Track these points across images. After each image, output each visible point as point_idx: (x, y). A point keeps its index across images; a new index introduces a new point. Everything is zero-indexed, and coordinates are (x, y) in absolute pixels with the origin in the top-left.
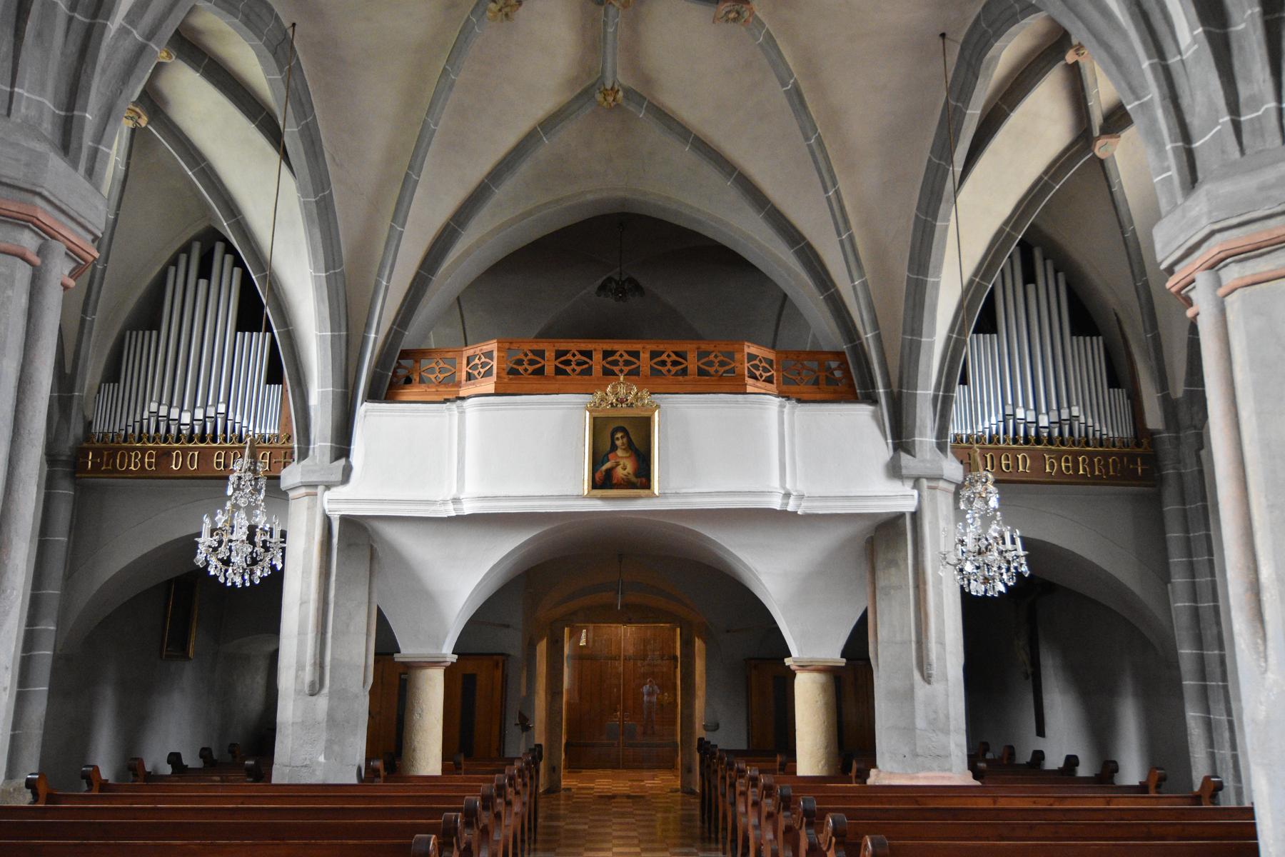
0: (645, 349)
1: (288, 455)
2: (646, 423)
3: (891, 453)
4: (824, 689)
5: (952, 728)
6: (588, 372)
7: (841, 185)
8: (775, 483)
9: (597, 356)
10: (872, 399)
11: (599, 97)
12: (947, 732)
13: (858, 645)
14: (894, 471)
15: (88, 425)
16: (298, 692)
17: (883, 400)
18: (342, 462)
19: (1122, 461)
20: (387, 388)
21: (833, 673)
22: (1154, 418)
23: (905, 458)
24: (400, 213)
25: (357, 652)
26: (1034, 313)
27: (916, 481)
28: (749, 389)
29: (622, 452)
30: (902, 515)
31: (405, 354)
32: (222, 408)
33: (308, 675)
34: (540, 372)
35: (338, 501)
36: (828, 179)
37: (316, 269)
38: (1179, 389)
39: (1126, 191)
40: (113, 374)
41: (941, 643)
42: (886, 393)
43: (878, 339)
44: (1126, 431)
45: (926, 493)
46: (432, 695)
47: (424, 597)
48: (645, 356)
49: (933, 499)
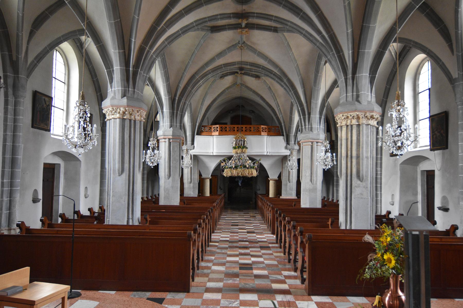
0: (244, 126)
1: (183, 144)
4: (274, 183)
6: (234, 131)
7: (278, 100)
8: (266, 150)
9: (236, 128)
10: (283, 135)
12: (292, 190)
13: (280, 177)
14: (286, 148)
16: (165, 177)
20: (199, 133)
21: (275, 180)
23: (288, 146)
24: (202, 104)
25: (196, 177)
27: (290, 150)
28: (262, 134)
31: (203, 126)
33: (189, 180)
34: (226, 131)
36: (275, 99)
41: (292, 176)
43: (285, 125)
47: (206, 168)
48: (244, 128)
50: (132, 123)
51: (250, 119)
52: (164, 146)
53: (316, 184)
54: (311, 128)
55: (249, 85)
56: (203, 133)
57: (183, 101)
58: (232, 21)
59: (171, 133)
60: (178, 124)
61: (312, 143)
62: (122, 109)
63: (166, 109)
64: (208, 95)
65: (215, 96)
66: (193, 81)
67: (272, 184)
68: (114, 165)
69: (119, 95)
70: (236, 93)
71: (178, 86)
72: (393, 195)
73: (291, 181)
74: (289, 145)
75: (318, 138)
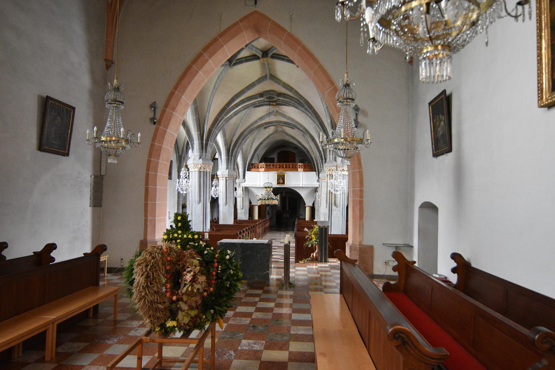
0: (284, 164)
2: (284, 176)
10: (316, 171)
13: (313, 204)
20: (249, 170)
24: (251, 147)
25: (247, 205)
29: (281, 179)
50: (205, 173)
51: (294, 154)
52: (222, 183)
55: (287, 132)
56: (253, 170)
57: (236, 149)
58: (268, 103)
59: (227, 173)
60: (232, 167)
62: (200, 166)
63: (224, 156)
64: (255, 143)
65: (261, 141)
66: (243, 136)
67: (308, 210)
68: (195, 198)
69: (197, 158)
70: (279, 137)
71: (232, 140)
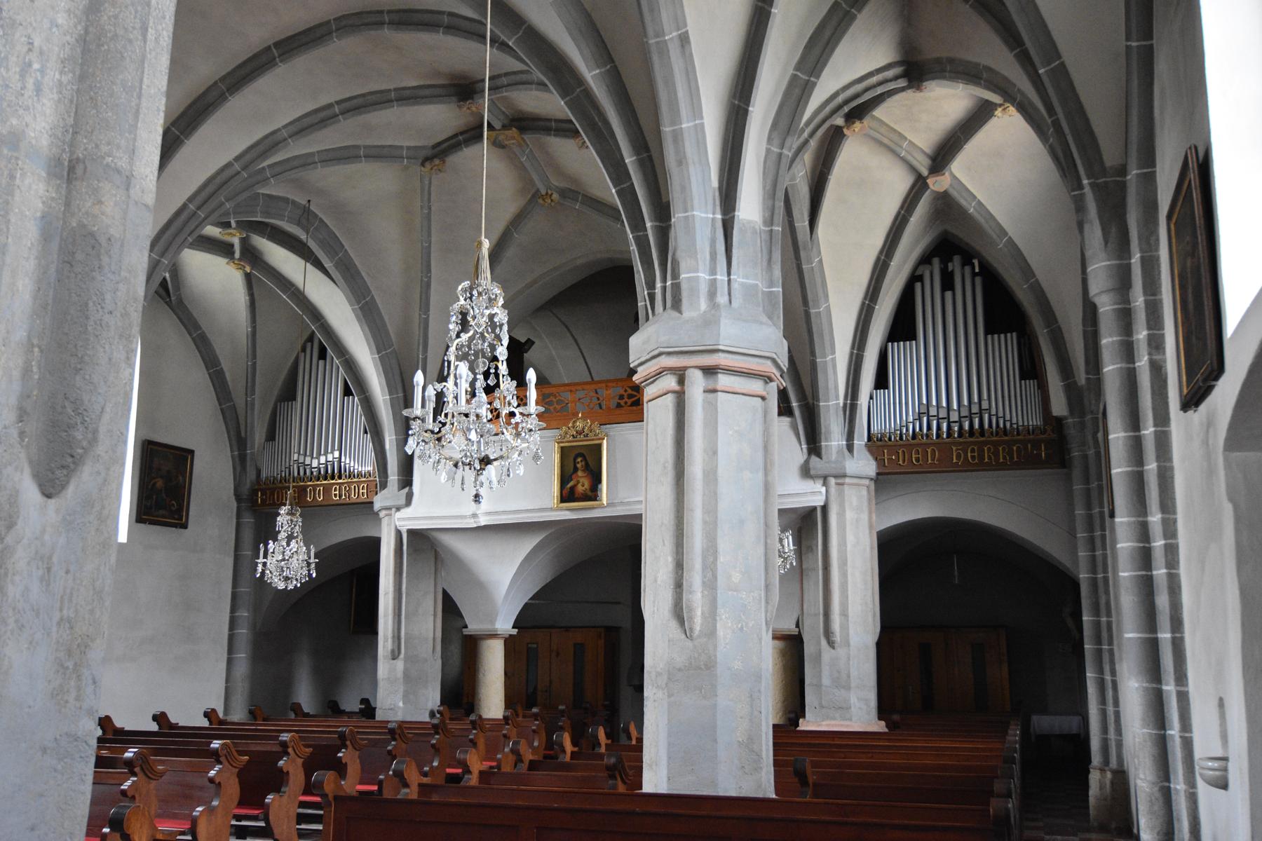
3: (806, 457)
5: (853, 685)
11: (540, 201)
14: (806, 472)
15: (259, 472)
17: (797, 412)
18: (406, 490)
19: (1026, 448)
22: (1059, 406)
23: (814, 459)
26: (950, 315)
27: (825, 479)
30: (814, 509)
32: (337, 454)
35: (404, 519)
37: (372, 353)
38: (1081, 377)
39: (989, 208)
40: (271, 436)
41: (844, 614)
42: (800, 406)
44: (1035, 421)
45: (833, 490)
46: (494, 661)
47: (479, 586)
49: (841, 494)
53: (711, 633)
54: (677, 288)
61: (681, 381)
72: (1221, 700)
73: (837, 638)
74: (819, 455)
75: (708, 343)
